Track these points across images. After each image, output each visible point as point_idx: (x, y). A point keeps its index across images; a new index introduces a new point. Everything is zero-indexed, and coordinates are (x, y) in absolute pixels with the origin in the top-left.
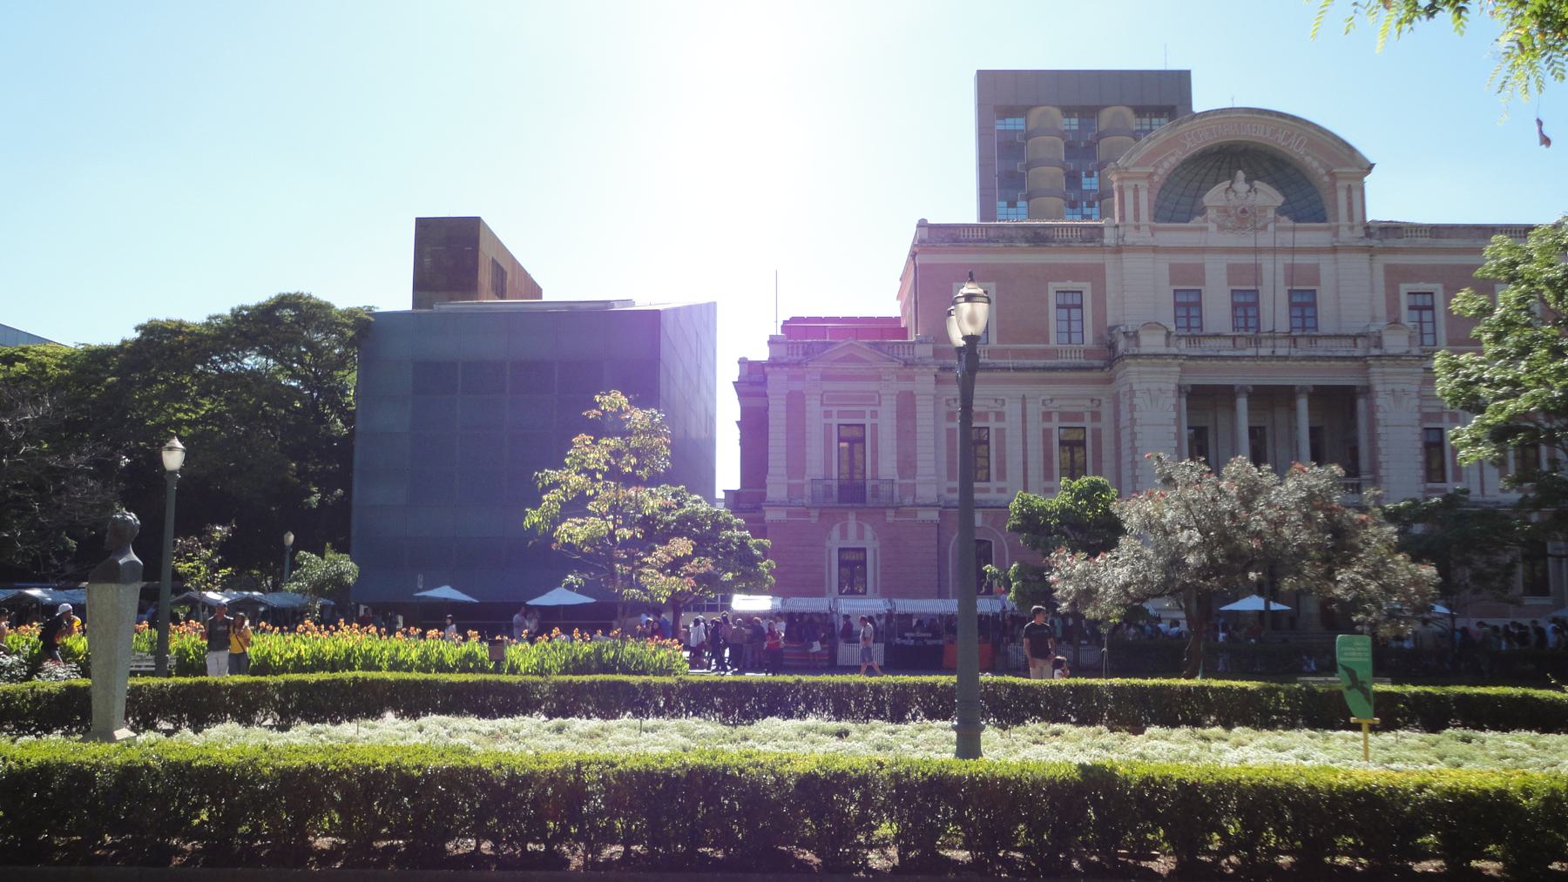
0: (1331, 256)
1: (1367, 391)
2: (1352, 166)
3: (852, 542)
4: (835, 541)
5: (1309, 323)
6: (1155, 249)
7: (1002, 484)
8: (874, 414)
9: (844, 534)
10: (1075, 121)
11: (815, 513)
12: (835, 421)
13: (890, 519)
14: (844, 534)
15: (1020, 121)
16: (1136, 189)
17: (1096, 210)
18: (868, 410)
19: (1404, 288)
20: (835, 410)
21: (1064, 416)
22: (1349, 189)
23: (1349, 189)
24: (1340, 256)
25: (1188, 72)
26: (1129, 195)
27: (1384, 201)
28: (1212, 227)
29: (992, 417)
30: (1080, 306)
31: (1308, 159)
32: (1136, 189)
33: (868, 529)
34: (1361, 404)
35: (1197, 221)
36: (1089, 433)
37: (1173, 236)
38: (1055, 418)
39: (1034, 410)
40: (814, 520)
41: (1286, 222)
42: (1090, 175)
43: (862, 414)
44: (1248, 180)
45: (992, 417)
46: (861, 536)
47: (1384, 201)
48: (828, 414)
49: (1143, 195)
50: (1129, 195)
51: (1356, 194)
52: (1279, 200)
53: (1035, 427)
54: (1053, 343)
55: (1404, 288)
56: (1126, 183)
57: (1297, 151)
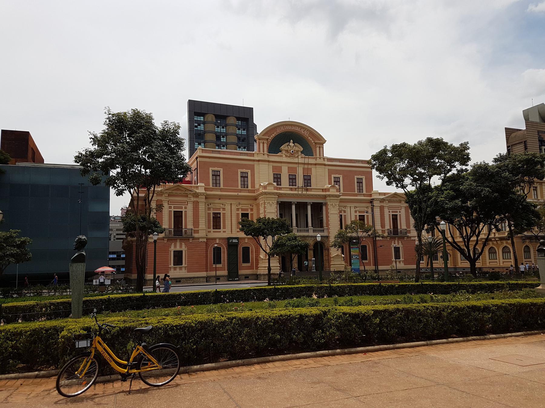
0: (314, 166)
1: (326, 204)
2: (320, 141)
3: (178, 248)
4: (172, 249)
5: (309, 184)
6: (269, 161)
7: (224, 230)
8: (186, 208)
9: (175, 246)
10: (240, 122)
11: (166, 239)
12: (391, 214)
13: (191, 241)
14: (175, 246)
15: (202, 118)
16: (263, 143)
17: (225, 148)
18: (183, 206)
19: (333, 176)
20: (173, 206)
21: (242, 210)
22: (320, 147)
23: (320, 147)
24: (260, 163)
25: (190, 101)
26: (261, 145)
27: (330, 151)
28: (284, 156)
29: (249, 210)
30: (219, 176)
31: (309, 138)
32: (263, 143)
33: (400, 243)
34: (324, 208)
35: (279, 154)
36: (221, 214)
37: (273, 158)
38: (240, 210)
39: (234, 207)
40: (166, 242)
41: (303, 155)
42: (223, 137)
43: (219, 209)
44: (293, 143)
45: (221, 209)
46: (398, 244)
47: (330, 151)
48: (170, 207)
49: (265, 145)
50: (261, 145)
51: (321, 149)
52: (302, 149)
53: (234, 213)
54: (356, 192)
55: (333, 176)
56: (260, 141)
57: (306, 134)
